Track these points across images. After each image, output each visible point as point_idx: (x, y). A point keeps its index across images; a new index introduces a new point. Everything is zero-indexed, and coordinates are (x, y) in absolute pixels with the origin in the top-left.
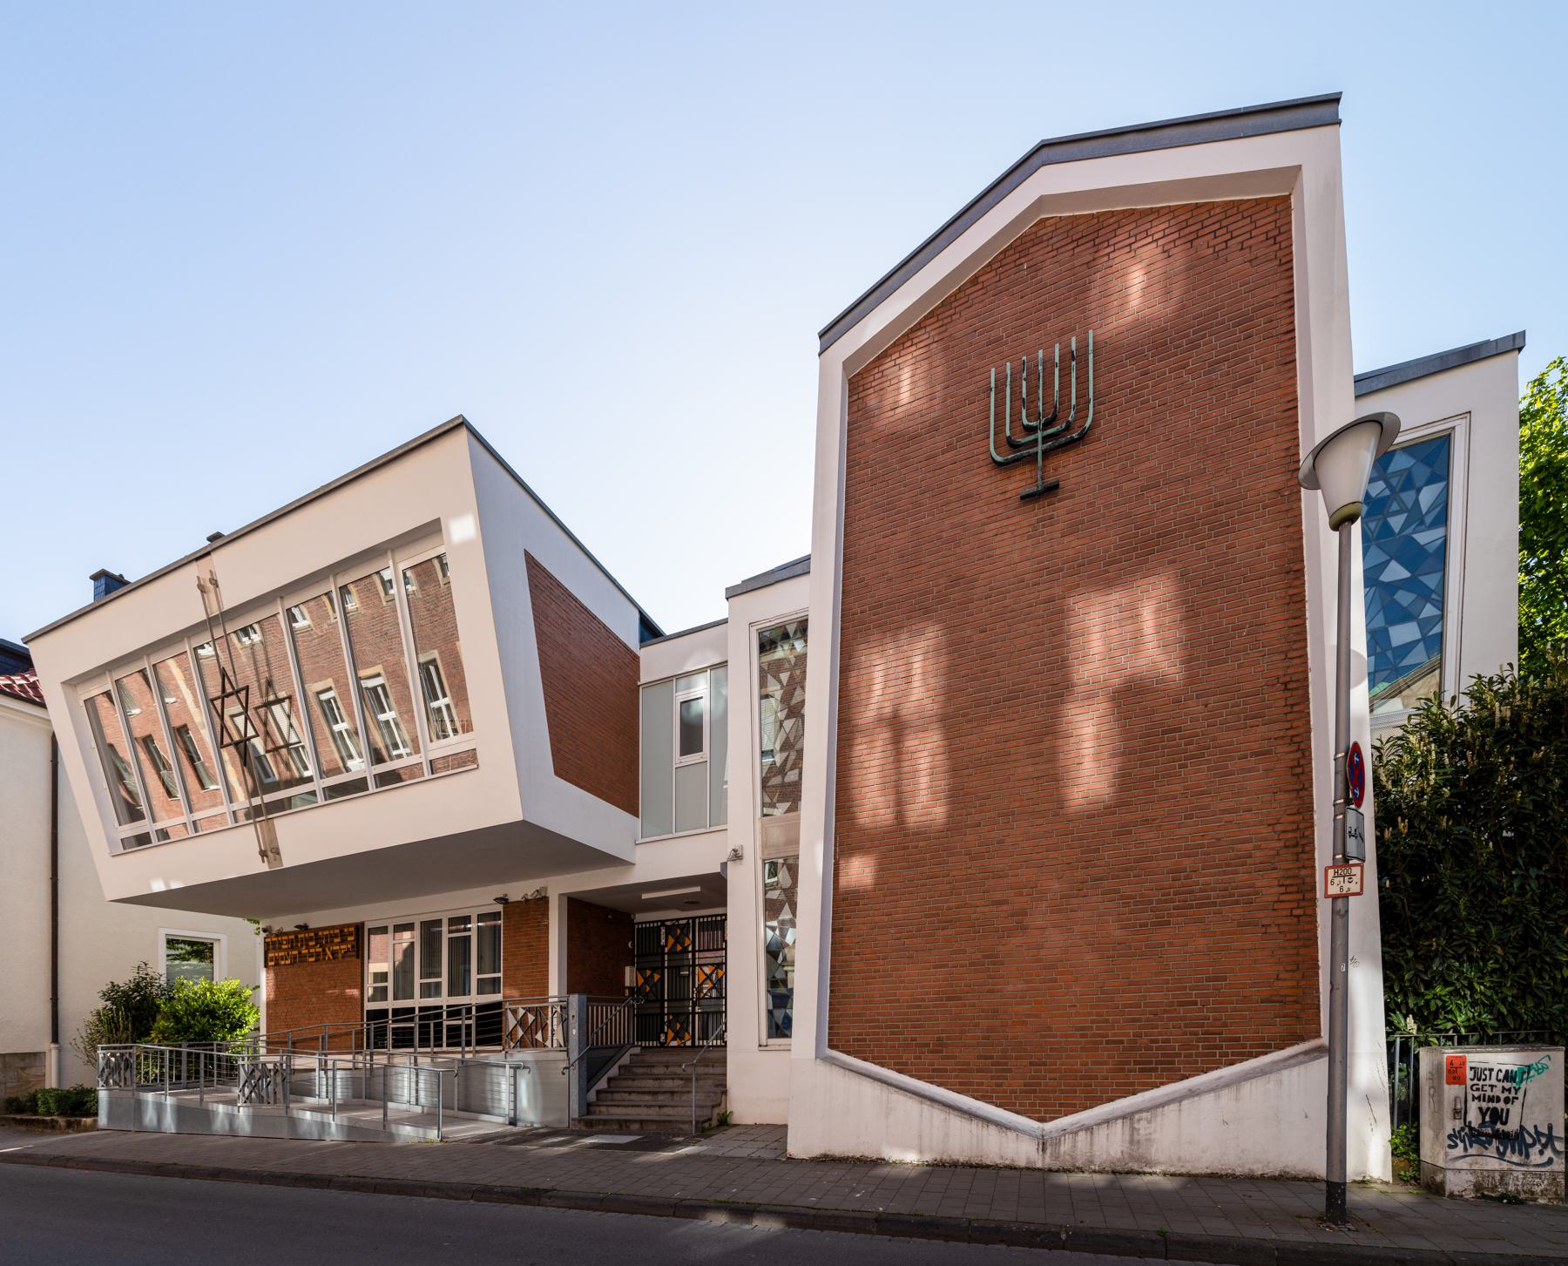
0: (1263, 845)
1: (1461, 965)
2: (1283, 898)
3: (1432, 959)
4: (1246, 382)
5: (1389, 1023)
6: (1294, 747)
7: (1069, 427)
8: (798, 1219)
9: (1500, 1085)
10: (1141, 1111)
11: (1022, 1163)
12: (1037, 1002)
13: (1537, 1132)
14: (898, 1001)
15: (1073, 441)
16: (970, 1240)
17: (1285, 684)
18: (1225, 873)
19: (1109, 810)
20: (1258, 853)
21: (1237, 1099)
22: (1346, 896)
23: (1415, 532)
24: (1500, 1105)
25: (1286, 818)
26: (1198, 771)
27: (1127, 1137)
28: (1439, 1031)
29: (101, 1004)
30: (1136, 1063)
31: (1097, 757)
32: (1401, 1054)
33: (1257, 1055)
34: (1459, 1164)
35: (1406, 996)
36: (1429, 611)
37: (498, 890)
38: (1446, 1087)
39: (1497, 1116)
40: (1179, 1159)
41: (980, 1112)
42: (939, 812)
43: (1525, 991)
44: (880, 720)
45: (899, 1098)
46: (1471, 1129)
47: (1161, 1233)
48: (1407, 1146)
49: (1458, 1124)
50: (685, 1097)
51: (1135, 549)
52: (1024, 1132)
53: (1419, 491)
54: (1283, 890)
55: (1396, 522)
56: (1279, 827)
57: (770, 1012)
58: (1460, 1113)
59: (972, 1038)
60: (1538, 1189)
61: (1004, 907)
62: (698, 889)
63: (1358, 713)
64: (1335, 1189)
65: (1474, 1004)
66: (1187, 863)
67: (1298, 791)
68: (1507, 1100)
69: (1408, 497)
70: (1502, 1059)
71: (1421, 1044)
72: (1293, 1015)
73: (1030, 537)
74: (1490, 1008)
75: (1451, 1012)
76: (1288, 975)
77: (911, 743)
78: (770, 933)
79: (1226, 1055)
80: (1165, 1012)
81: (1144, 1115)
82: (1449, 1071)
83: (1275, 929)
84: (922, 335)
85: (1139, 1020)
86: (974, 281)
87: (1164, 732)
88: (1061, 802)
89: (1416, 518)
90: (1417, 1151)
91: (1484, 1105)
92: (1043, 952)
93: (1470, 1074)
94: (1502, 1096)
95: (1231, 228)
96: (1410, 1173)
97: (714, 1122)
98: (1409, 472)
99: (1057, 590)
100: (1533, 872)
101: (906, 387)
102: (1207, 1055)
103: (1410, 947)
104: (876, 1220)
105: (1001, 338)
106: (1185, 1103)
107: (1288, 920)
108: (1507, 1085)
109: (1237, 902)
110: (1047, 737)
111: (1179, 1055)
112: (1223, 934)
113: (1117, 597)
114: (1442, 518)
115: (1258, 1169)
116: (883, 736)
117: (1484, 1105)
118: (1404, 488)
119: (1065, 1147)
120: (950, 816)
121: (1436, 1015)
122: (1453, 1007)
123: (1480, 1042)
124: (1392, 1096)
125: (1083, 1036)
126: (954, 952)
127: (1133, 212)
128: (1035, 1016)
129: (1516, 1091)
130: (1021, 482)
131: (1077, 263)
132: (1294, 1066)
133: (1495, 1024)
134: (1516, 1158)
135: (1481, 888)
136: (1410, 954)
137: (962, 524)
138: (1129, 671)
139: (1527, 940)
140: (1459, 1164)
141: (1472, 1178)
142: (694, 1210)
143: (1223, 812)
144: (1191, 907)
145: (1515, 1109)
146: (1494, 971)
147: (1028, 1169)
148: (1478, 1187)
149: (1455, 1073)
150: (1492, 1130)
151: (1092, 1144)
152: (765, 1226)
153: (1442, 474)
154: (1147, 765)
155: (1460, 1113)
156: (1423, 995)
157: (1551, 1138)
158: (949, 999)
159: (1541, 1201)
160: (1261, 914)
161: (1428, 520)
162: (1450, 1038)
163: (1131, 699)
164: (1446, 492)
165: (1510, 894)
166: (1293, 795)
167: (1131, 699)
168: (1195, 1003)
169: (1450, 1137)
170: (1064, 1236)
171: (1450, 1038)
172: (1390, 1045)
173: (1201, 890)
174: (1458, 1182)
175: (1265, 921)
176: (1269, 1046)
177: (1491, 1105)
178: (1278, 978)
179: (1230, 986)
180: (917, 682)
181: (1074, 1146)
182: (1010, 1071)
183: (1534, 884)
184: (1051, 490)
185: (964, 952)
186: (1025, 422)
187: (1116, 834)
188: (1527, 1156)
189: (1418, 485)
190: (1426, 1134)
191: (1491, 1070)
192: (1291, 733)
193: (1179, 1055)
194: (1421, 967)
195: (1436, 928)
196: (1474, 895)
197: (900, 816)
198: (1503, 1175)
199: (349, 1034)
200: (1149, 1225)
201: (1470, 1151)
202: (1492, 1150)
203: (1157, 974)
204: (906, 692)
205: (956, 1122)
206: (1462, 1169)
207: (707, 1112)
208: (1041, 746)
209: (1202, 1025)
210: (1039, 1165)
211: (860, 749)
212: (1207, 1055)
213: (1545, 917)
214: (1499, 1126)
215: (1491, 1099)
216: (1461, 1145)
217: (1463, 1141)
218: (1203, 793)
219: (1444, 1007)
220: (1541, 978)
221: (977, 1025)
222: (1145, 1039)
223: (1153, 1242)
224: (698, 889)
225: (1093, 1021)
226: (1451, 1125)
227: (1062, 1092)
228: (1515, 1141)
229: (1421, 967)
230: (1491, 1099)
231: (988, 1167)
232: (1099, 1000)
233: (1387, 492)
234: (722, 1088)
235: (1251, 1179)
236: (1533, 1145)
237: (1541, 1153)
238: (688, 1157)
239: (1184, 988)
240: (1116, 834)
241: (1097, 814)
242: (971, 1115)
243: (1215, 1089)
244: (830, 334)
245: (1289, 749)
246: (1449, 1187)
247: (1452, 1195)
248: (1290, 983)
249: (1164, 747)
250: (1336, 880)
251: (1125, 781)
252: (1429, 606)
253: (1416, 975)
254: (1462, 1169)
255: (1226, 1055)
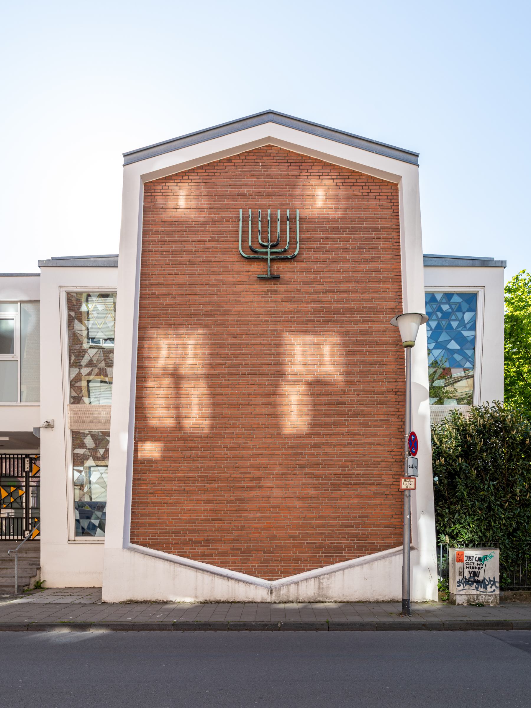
0: (385, 460)
1: (466, 517)
2: (394, 483)
3: (456, 513)
4: (378, 257)
5: (438, 538)
6: (400, 420)
7: (285, 251)
9: (476, 563)
10: (324, 574)
11: (259, 600)
12: (267, 523)
13: (490, 580)
14: (180, 519)
15: (287, 259)
16: (229, 630)
17: (396, 392)
18: (367, 470)
19: (308, 436)
20: (383, 463)
21: (371, 569)
22: (409, 490)
23: (462, 330)
24: (477, 570)
25: (395, 450)
26: (354, 424)
27: (317, 587)
28: (459, 542)
30: (322, 553)
31: (300, 410)
32: (442, 550)
33: (383, 550)
34: (461, 593)
35: (445, 527)
36: (468, 365)
38: (456, 563)
39: (475, 574)
40: (343, 595)
41: (233, 576)
42: (205, 425)
43: (489, 527)
44: (166, 372)
45: (179, 569)
46: (466, 579)
47: (328, 622)
48: (444, 588)
49: (461, 577)
50: (9, 571)
51: (322, 317)
52: (260, 585)
53: (464, 313)
54: (394, 480)
55: (454, 324)
56: (393, 453)
57: (77, 521)
58: (461, 573)
59: (229, 540)
60: (490, 601)
61: (248, 476)
62: (7, 439)
63: (423, 415)
64: (406, 603)
65: (471, 532)
66: (349, 464)
67: (401, 439)
68: (479, 568)
69: (459, 315)
70: (475, 553)
71: (451, 547)
72: (395, 535)
73: (263, 297)
74: (476, 533)
75: (461, 534)
76: (397, 516)
77: (186, 386)
78: (77, 474)
79: (368, 550)
80: (338, 530)
81: (326, 576)
82: (457, 557)
83: (391, 497)
84: (193, 176)
85: (324, 533)
86: (229, 160)
87: (337, 404)
89: (462, 324)
90: (448, 589)
91: (471, 570)
92: (271, 499)
93: (465, 558)
94: (477, 567)
95: (370, 187)
96: (446, 598)
97: (32, 586)
98: (460, 304)
99: (279, 327)
100: (491, 483)
102: (359, 550)
103: (447, 508)
104: (173, 625)
105: (246, 194)
106: (346, 571)
107: (397, 493)
108: (479, 563)
109: (373, 484)
110: (271, 396)
111: (345, 550)
112: (366, 496)
113: (309, 338)
114: (473, 328)
115: (381, 599)
116: (167, 381)
117: (471, 570)
119: (283, 592)
120: (212, 427)
121: (457, 535)
122: (463, 533)
123: (474, 546)
124: (438, 568)
125: (293, 540)
126: (218, 496)
127: (321, 161)
128: (267, 530)
129: (482, 565)
130: (257, 269)
131: (290, 173)
132: (398, 555)
133: (478, 539)
134: (482, 590)
135: (473, 488)
136: (447, 511)
137: (222, 280)
138: (318, 373)
139: (489, 508)
140: (461, 593)
141: (466, 598)
142: (52, 626)
143: (366, 443)
144: (351, 484)
145: (482, 571)
146: (477, 520)
147: (262, 602)
148: (468, 601)
149: (460, 558)
150: (474, 580)
151: (298, 590)
153: (473, 309)
154: (328, 417)
155: (461, 573)
156: (451, 527)
157: (494, 582)
158: (213, 520)
159: (491, 605)
160: (385, 489)
161: (468, 326)
162: (462, 545)
163: (317, 387)
164: (475, 316)
165: (483, 491)
166: (400, 440)
167: (317, 387)
168: (353, 527)
169: (458, 582)
170: (279, 625)
171: (462, 545)
172: (438, 547)
173: (356, 477)
174: (460, 599)
175: (386, 493)
176: (388, 546)
177: (473, 570)
178: (392, 518)
179: (370, 520)
180: (190, 355)
181: (288, 591)
182: (252, 556)
183: (492, 488)
184: (275, 278)
185: (223, 496)
186: (260, 242)
187: (312, 447)
188: (486, 589)
189: (464, 311)
190: (451, 581)
191: (473, 557)
192: (398, 413)
193: (345, 550)
194: (451, 516)
195: (457, 501)
196: (470, 490)
197: (179, 423)
198: (478, 596)
200: (322, 619)
201: (466, 588)
202: (473, 587)
203: (333, 513)
204: (184, 359)
205: (218, 581)
206: (462, 594)
207: (25, 581)
208: (270, 400)
209: (356, 537)
210: (269, 600)
211: (151, 384)
212: (359, 550)
213: (497, 500)
214: (476, 578)
215: (473, 568)
216: (462, 585)
217: (463, 584)
218: (356, 434)
219: (460, 533)
220: (495, 523)
221: (232, 533)
222: (328, 542)
223: (323, 625)
224: (7, 439)
225: (299, 533)
226: (458, 578)
227: (282, 566)
228: (481, 583)
229: (451, 516)
230: (473, 568)
231: (238, 602)
232: (303, 523)
233: (450, 310)
234: (36, 566)
235: (377, 602)
236: (488, 585)
237: (491, 587)
238: (19, 604)
239: (348, 520)
240: (312, 447)
241: (298, 438)
242: (228, 578)
243: (361, 564)
245: (397, 420)
246: (457, 602)
247: (458, 605)
248: (398, 520)
249: (337, 410)
250: (405, 483)
251: (315, 423)
252: (468, 363)
253: (449, 519)
254: (462, 594)
255: (368, 550)
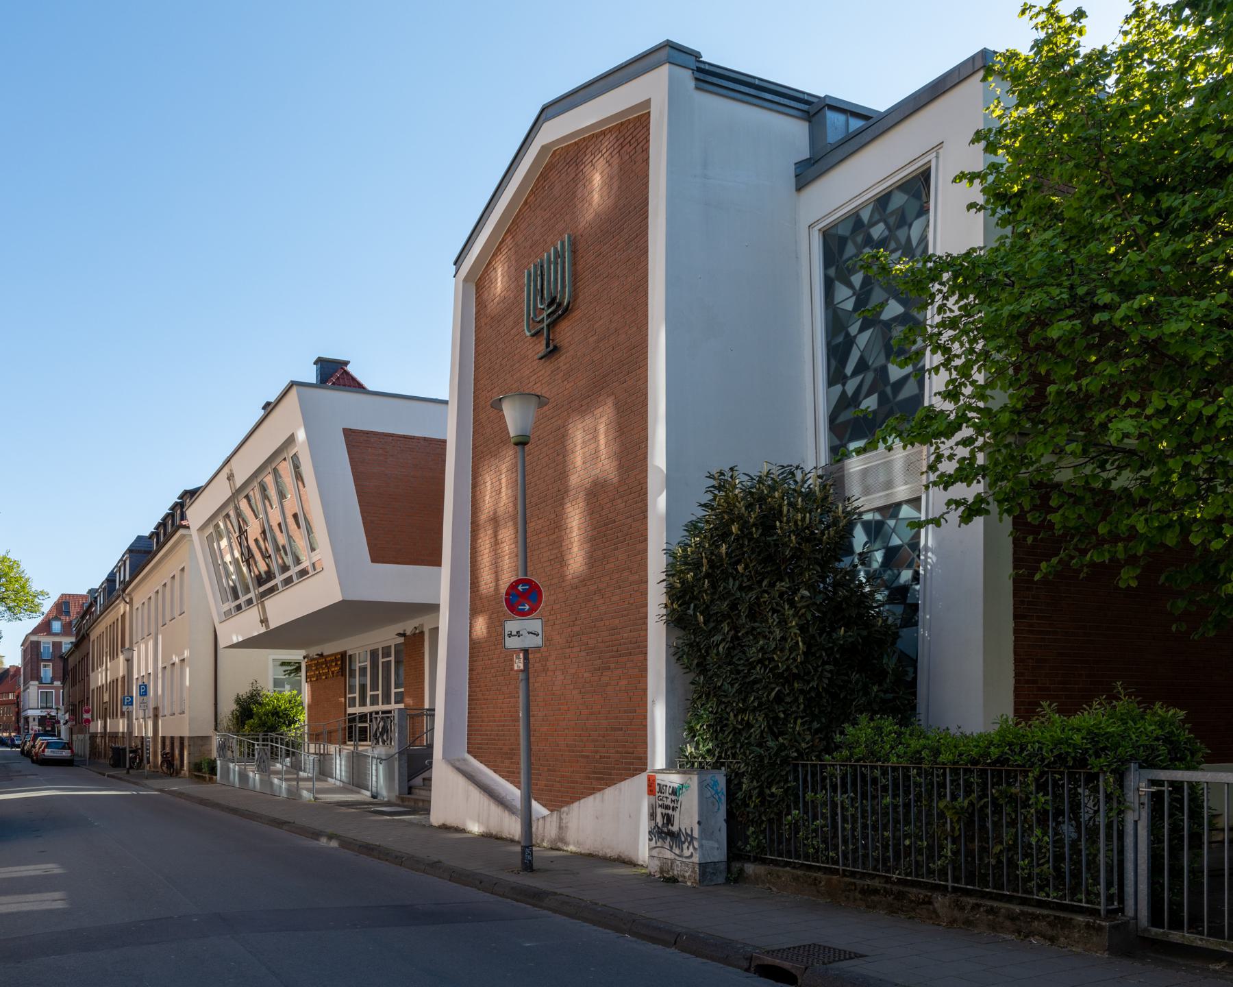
8: (346, 843)
29: (235, 707)
37: (399, 628)
53: (910, 226)
60: (687, 875)
88: (563, 577)
101: (500, 281)
118: (899, 226)
142: (316, 835)
152: (334, 844)
199: (336, 731)
233: (886, 233)
244: (458, 262)
